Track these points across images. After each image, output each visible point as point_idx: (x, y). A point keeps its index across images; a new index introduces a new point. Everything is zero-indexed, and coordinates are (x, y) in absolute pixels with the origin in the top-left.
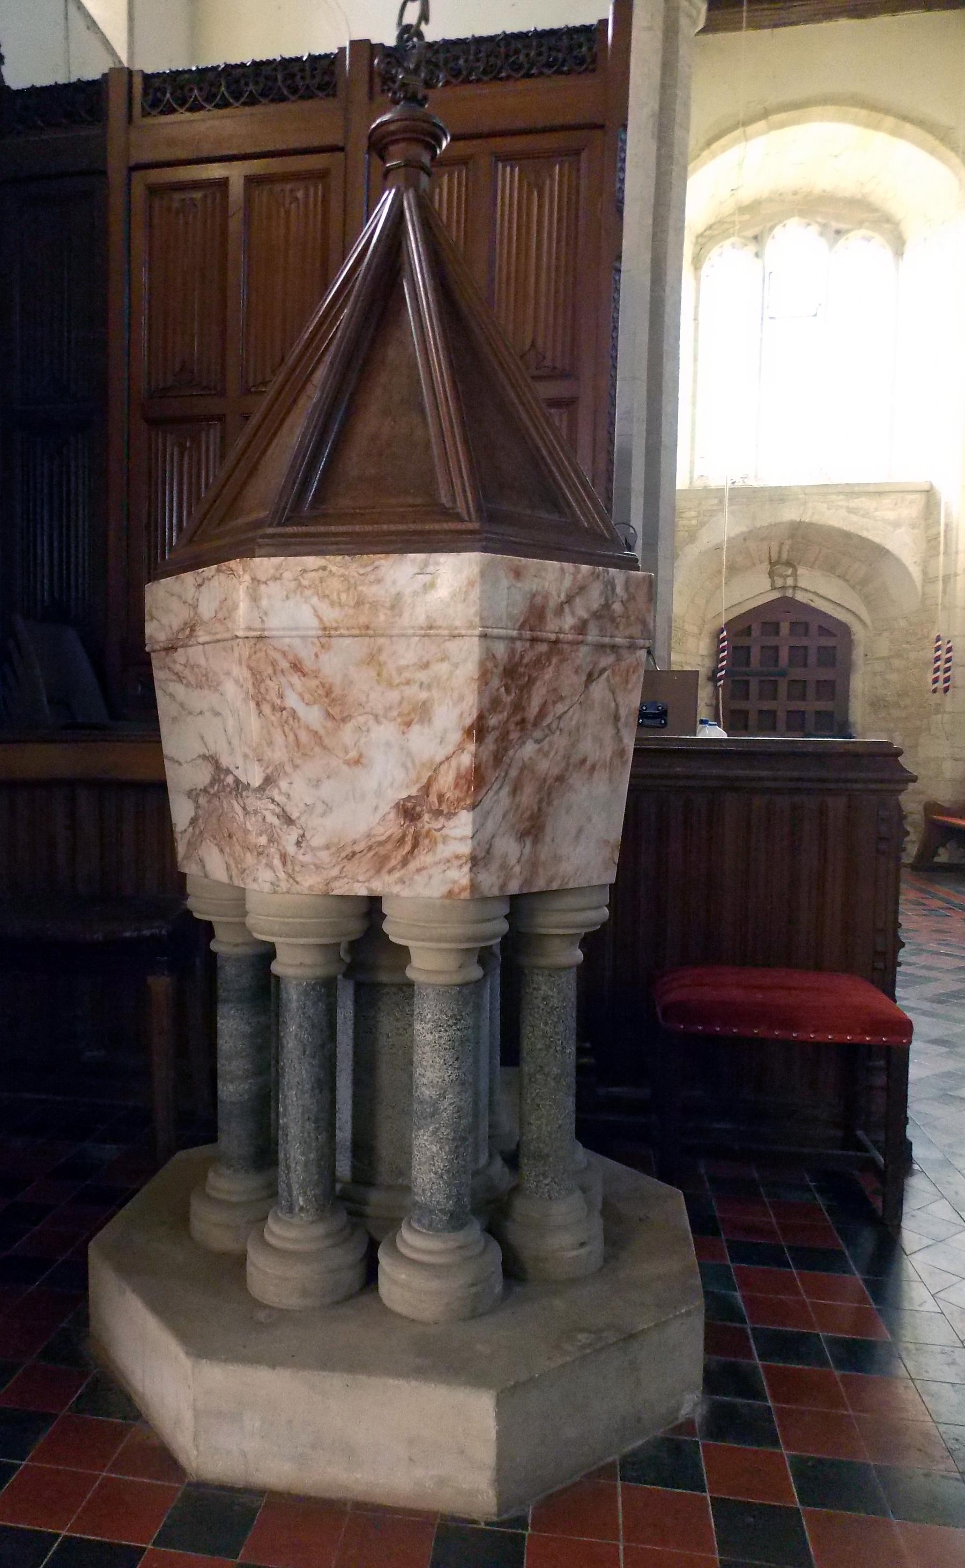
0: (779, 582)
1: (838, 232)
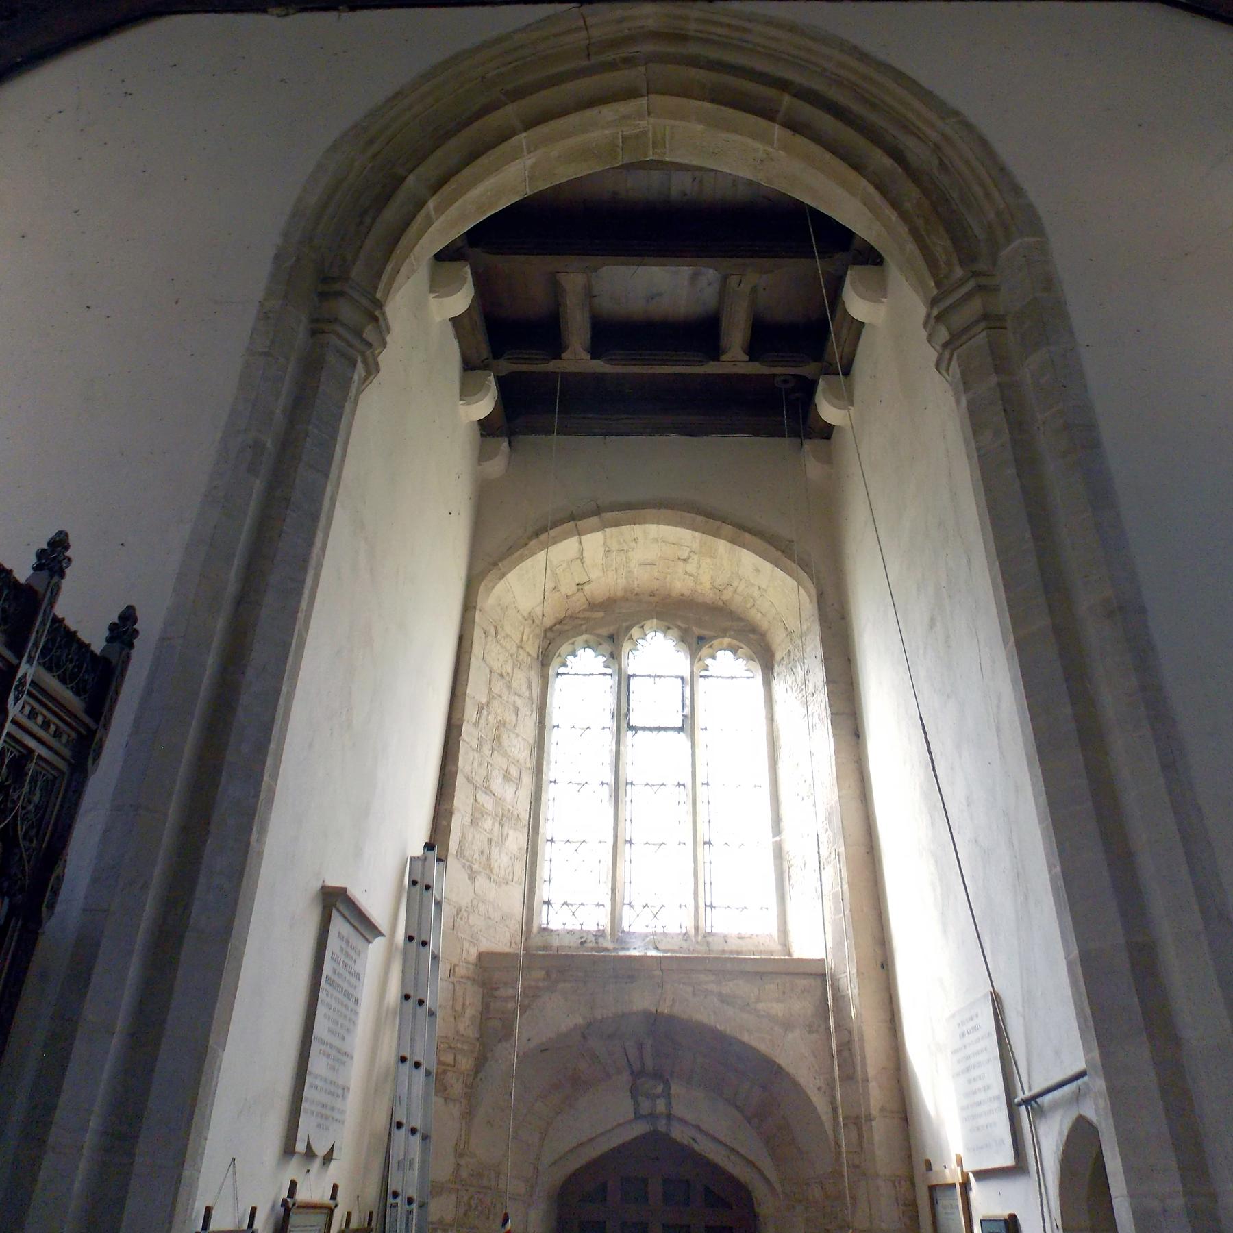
0: (645, 1107)
1: (701, 639)
